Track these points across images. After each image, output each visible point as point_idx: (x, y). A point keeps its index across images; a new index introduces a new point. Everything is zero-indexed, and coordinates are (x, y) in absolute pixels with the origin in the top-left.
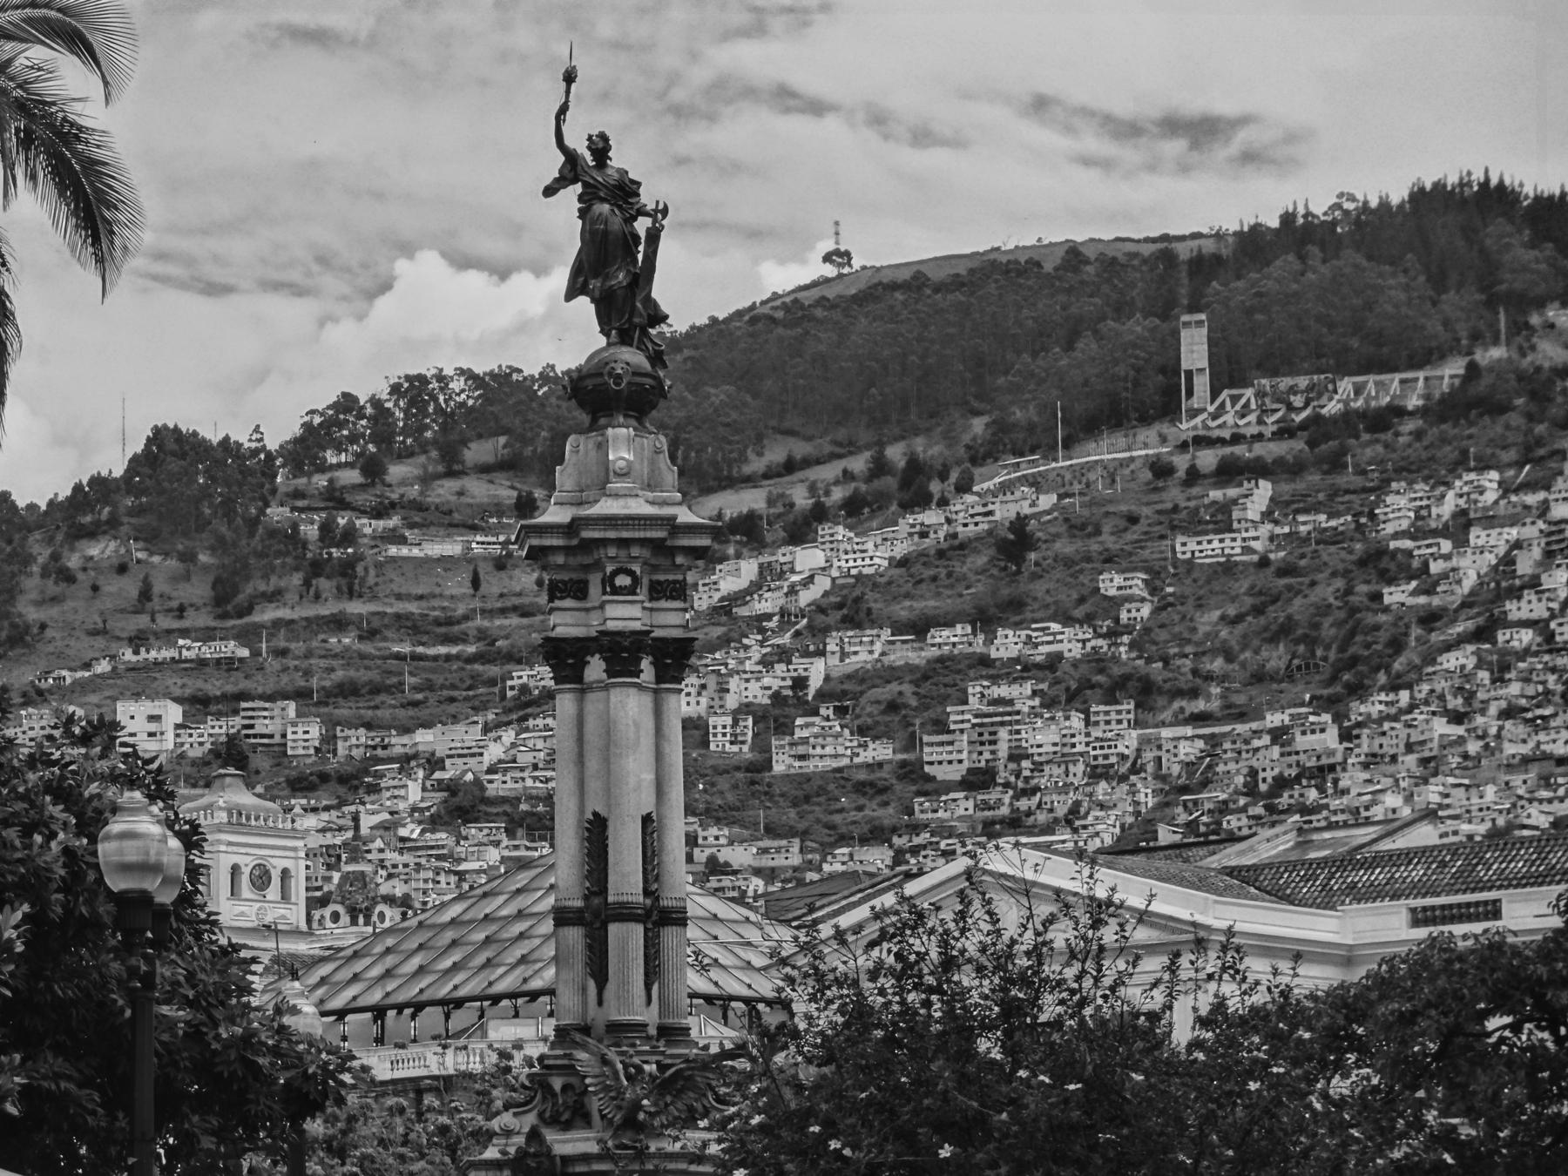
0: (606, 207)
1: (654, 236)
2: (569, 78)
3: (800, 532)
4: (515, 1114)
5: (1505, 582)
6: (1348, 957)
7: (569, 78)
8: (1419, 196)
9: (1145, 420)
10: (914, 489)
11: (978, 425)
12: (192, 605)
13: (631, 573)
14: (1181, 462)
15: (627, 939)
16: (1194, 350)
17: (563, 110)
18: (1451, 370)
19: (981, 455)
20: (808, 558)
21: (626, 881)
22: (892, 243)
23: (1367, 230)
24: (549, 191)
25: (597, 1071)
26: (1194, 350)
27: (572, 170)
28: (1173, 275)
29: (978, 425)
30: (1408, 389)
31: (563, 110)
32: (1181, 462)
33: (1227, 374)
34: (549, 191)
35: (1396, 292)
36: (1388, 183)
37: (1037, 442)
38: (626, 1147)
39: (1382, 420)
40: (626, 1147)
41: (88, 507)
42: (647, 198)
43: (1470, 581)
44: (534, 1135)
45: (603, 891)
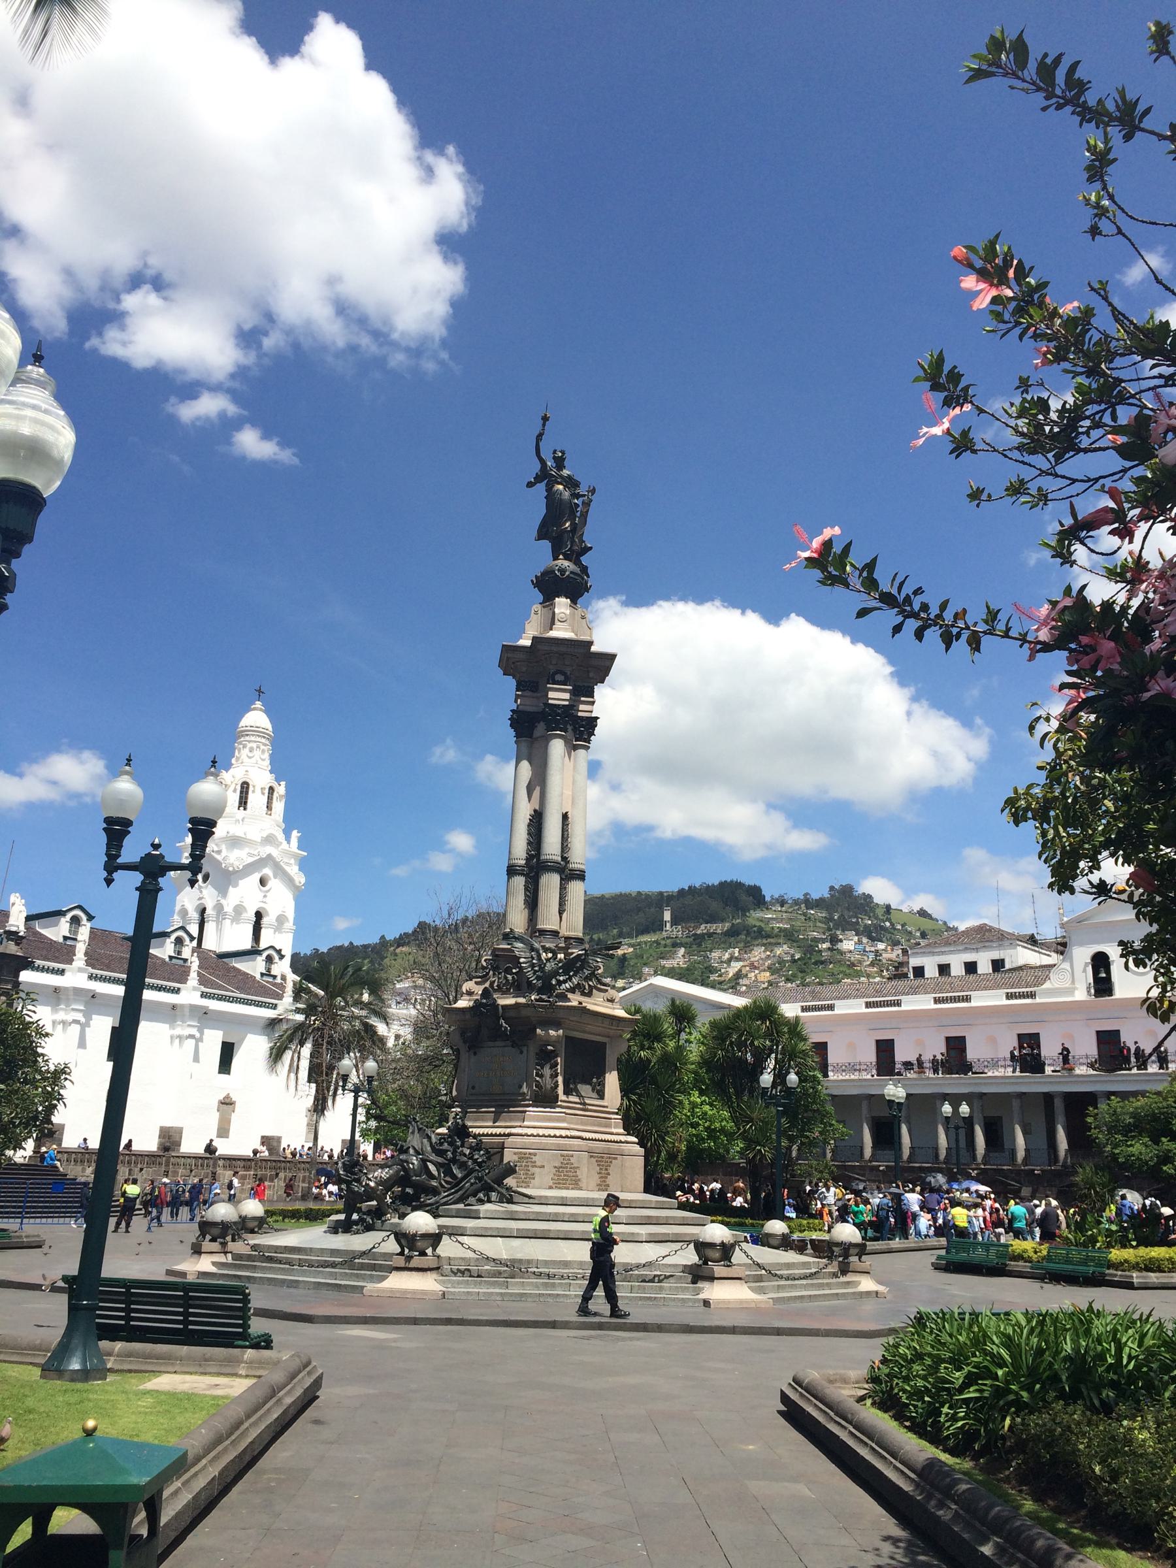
0: (561, 487)
1: (587, 504)
2: (545, 419)
4: (476, 983)
5: (739, 975)
7: (545, 419)
8: (721, 884)
9: (654, 931)
11: (615, 931)
12: (136, 281)
13: (564, 674)
14: (663, 942)
15: (550, 883)
16: (667, 916)
17: (539, 437)
18: (727, 925)
21: (551, 847)
23: (709, 890)
24: (530, 485)
25: (528, 955)
26: (667, 916)
27: (543, 476)
29: (615, 931)
30: (719, 928)
31: (539, 437)
32: (663, 942)
33: (675, 921)
34: (530, 485)
35: (715, 905)
36: (715, 881)
37: (630, 936)
38: (543, 1001)
39: (710, 935)
40: (543, 1001)
41: (402, 941)
43: (731, 975)
44: (486, 993)
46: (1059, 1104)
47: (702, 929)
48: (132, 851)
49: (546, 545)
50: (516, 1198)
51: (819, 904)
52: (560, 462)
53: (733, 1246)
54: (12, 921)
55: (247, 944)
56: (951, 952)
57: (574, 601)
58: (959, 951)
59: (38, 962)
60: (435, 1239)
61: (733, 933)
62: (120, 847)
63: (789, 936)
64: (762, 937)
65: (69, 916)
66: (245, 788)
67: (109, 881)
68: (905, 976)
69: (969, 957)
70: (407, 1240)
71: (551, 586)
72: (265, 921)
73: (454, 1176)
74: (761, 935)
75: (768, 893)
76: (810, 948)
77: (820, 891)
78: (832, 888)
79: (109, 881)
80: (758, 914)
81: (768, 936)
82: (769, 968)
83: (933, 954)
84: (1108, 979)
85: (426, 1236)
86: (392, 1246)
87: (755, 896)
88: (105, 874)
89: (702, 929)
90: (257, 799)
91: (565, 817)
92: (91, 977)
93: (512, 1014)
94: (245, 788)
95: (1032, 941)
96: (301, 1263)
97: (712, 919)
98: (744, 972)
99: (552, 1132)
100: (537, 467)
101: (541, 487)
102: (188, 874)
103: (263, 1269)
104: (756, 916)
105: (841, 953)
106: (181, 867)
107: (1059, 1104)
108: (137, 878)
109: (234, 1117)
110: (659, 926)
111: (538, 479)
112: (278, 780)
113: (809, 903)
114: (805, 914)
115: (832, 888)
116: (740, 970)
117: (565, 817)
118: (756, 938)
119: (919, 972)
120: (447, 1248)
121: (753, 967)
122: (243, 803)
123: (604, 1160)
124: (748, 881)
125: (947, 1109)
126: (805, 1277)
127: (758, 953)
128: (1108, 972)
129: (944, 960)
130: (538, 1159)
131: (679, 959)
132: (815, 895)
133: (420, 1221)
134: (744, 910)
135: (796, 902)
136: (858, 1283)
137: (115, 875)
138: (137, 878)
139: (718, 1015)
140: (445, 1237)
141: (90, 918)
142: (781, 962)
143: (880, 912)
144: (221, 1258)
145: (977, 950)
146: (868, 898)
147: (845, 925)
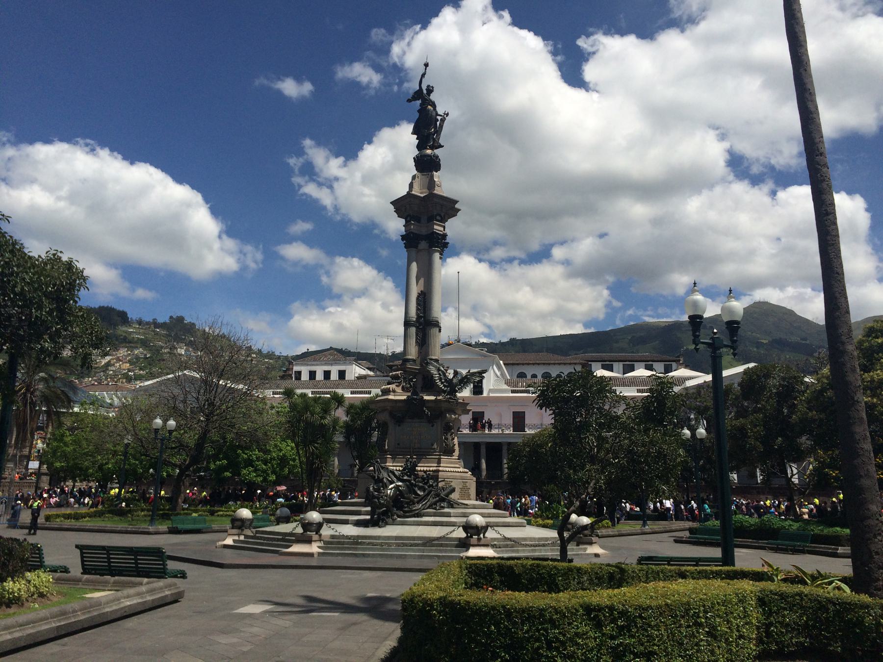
2: (426, 65)
8: (100, 307)
31: (423, 75)
46: (483, 451)
51: (163, 326)
56: (317, 365)
58: (322, 365)
60: (485, 528)
63: (144, 343)
64: (126, 342)
68: (291, 376)
69: (327, 368)
70: (307, 526)
74: (127, 342)
76: (157, 351)
77: (163, 319)
78: (171, 317)
80: (125, 329)
81: (130, 342)
82: (129, 361)
83: (307, 365)
87: (123, 317)
93: (430, 405)
96: (369, 544)
98: (112, 362)
99: (452, 469)
104: (122, 329)
107: (483, 451)
113: (156, 324)
114: (154, 331)
115: (171, 317)
116: (109, 361)
118: (122, 343)
120: (490, 534)
121: (118, 360)
124: (120, 308)
126: (531, 546)
127: (122, 352)
129: (313, 368)
132: (161, 320)
133: (314, 516)
134: (115, 325)
135: (148, 323)
136: (585, 549)
140: (325, 525)
142: (137, 358)
143: (199, 334)
144: (236, 538)
145: (332, 365)
147: (178, 339)
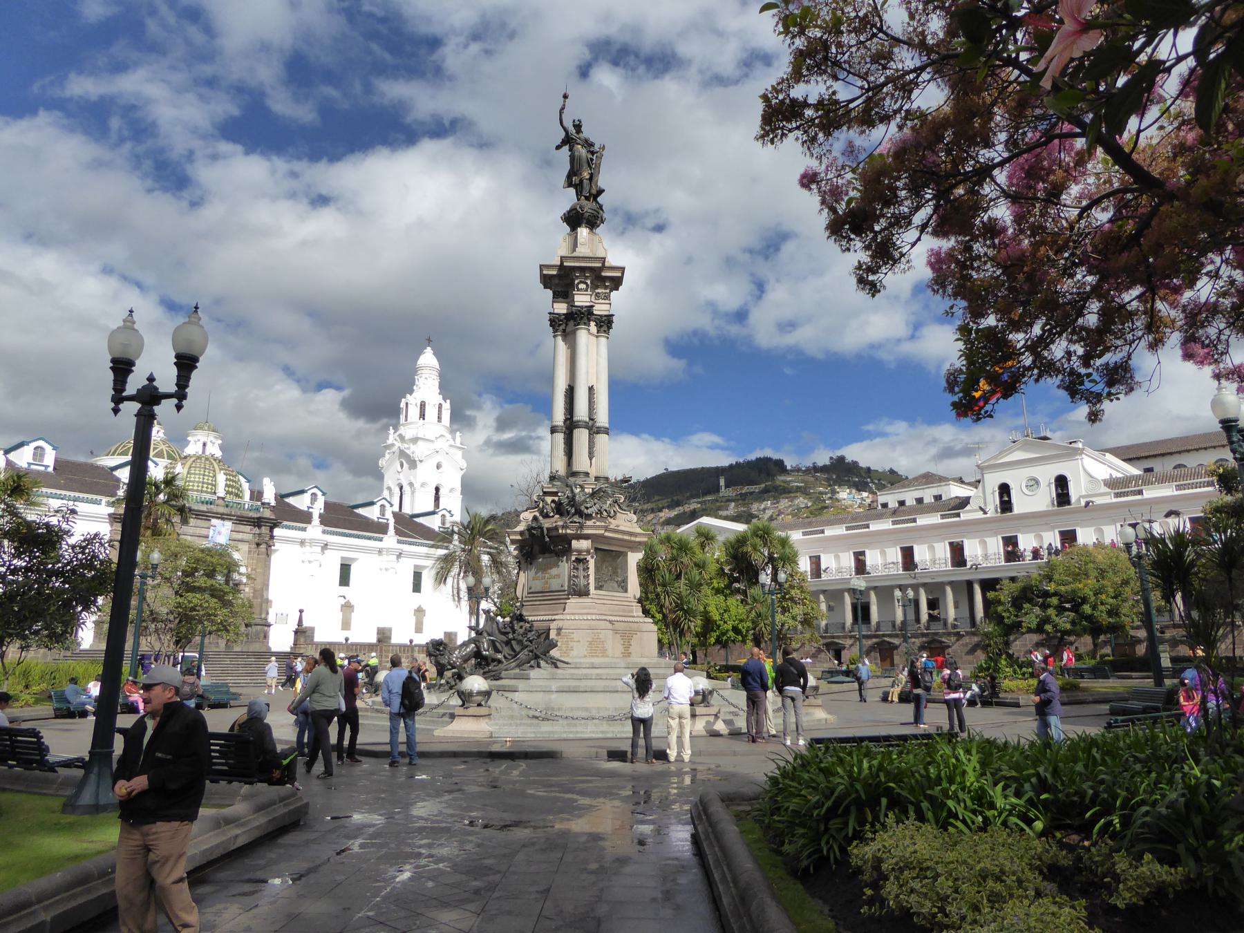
2: (565, 97)
3: (660, 511)
6: (84, 841)
7: (565, 97)
10: (678, 504)
15: (581, 436)
16: (722, 482)
17: (563, 109)
19: (688, 498)
20: (661, 514)
22: (674, 468)
24: (558, 147)
26: (722, 482)
27: (568, 141)
28: (718, 472)
30: (756, 488)
31: (563, 109)
33: (727, 486)
34: (558, 147)
37: (697, 496)
39: (751, 493)
42: (614, 294)
45: (572, 416)
47: (746, 489)
48: (134, 383)
49: (572, 191)
50: (559, 664)
52: (578, 127)
53: (711, 692)
54: (265, 496)
55: (431, 508)
57: (591, 229)
59: (285, 523)
61: (766, 491)
62: (124, 382)
65: (310, 492)
66: (423, 406)
67: (116, 411)
69: (918, 494)
70: (466, 697)
71: (574, 219)
72: (441, 492)
73: (513, 650)
74: (785, 491)
75: (789, 464)
79: (116, 411)
84: (1009, 502)
85: (480, 693)
86: (456, 701)
88: (113, 405)
89: (746, 489)
90: (431, 412)
91: (591, 389)
92: (324, 532)
94: (423, 406)
95: (961, 481)
97: (751, 483)
100: (563, 134)
101: (566, 148)
102: (175, 401)
103: (372, 718)
104: (781, 479)
105: (838, 500)
106: (168, 396)
108: (135, 406)
109: (425, 620)
110: (717, 489)
111: (564, 143)
112: (445, 400)
117: (591, 389)
119: (885, 505)
122: (422, 415)
123: (627, 637)
125: (898, 593)
127: (784, 503)
128: (1009, 496)
130: (576, 636)
131: (732, 509)
132: (820, 464)
137: (121, 406)
138: (135, 406)
139: (732, 538)
141: (324, 494)
142: (799, 509)
146: (855, 463)
